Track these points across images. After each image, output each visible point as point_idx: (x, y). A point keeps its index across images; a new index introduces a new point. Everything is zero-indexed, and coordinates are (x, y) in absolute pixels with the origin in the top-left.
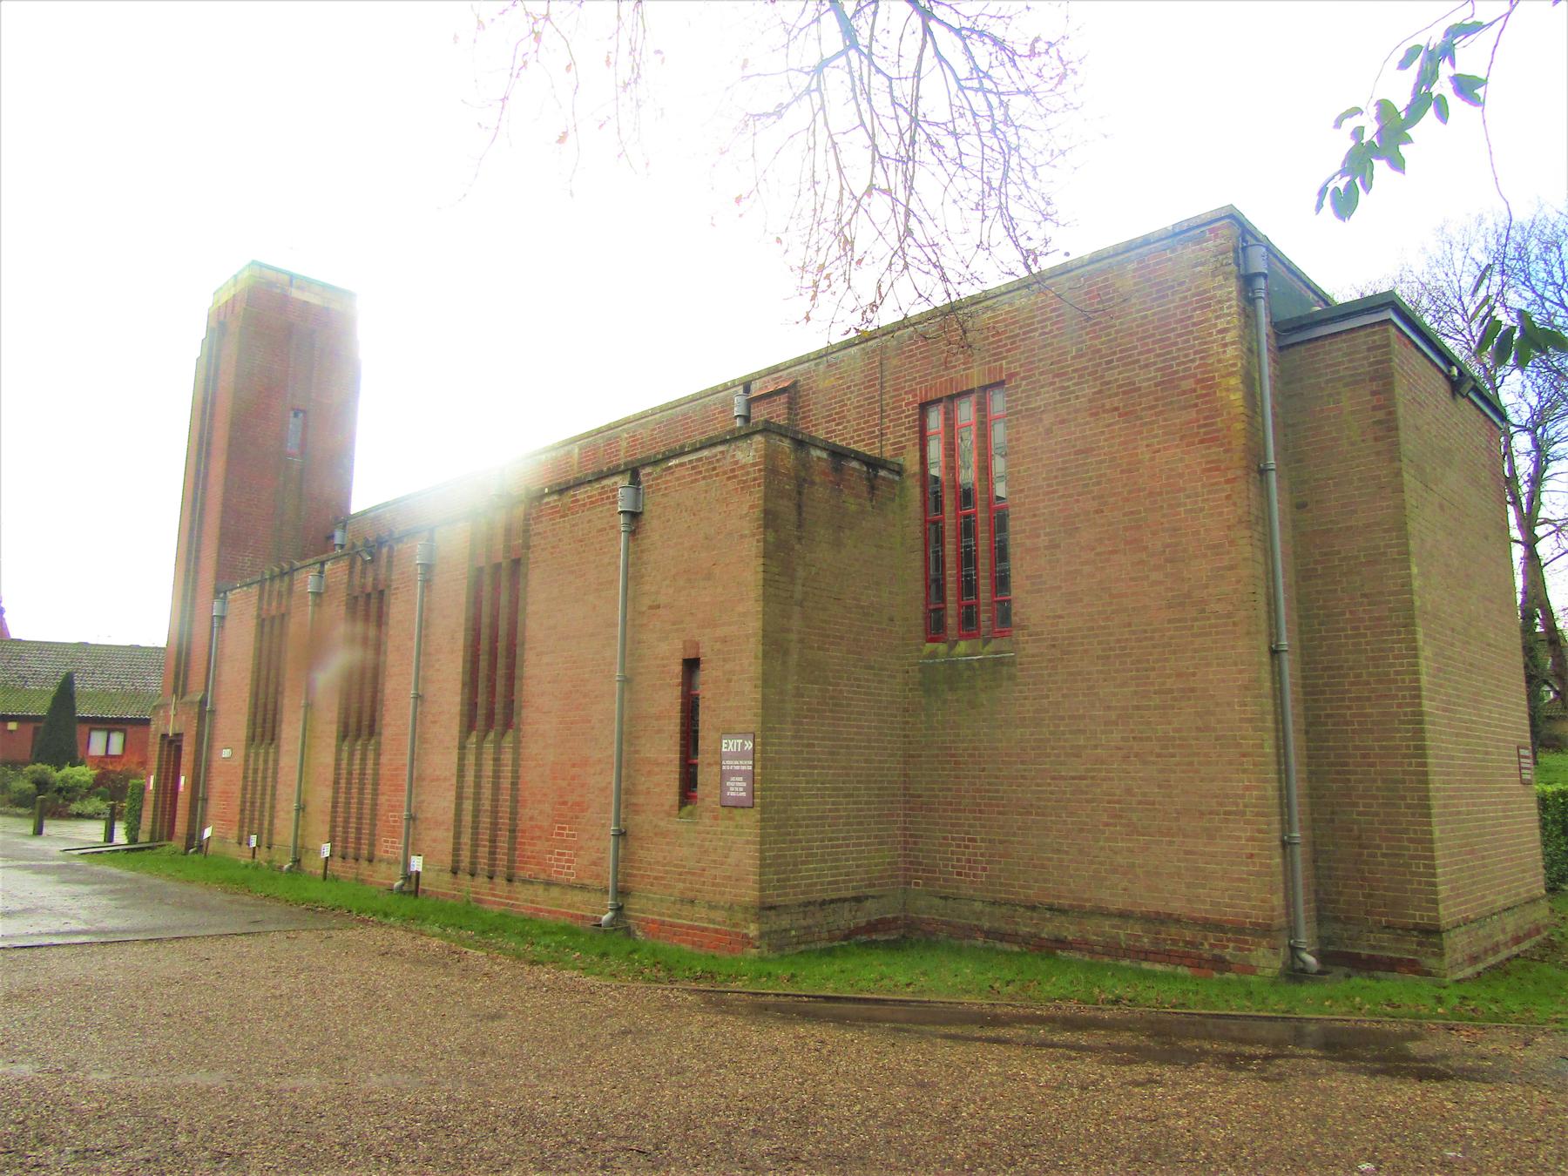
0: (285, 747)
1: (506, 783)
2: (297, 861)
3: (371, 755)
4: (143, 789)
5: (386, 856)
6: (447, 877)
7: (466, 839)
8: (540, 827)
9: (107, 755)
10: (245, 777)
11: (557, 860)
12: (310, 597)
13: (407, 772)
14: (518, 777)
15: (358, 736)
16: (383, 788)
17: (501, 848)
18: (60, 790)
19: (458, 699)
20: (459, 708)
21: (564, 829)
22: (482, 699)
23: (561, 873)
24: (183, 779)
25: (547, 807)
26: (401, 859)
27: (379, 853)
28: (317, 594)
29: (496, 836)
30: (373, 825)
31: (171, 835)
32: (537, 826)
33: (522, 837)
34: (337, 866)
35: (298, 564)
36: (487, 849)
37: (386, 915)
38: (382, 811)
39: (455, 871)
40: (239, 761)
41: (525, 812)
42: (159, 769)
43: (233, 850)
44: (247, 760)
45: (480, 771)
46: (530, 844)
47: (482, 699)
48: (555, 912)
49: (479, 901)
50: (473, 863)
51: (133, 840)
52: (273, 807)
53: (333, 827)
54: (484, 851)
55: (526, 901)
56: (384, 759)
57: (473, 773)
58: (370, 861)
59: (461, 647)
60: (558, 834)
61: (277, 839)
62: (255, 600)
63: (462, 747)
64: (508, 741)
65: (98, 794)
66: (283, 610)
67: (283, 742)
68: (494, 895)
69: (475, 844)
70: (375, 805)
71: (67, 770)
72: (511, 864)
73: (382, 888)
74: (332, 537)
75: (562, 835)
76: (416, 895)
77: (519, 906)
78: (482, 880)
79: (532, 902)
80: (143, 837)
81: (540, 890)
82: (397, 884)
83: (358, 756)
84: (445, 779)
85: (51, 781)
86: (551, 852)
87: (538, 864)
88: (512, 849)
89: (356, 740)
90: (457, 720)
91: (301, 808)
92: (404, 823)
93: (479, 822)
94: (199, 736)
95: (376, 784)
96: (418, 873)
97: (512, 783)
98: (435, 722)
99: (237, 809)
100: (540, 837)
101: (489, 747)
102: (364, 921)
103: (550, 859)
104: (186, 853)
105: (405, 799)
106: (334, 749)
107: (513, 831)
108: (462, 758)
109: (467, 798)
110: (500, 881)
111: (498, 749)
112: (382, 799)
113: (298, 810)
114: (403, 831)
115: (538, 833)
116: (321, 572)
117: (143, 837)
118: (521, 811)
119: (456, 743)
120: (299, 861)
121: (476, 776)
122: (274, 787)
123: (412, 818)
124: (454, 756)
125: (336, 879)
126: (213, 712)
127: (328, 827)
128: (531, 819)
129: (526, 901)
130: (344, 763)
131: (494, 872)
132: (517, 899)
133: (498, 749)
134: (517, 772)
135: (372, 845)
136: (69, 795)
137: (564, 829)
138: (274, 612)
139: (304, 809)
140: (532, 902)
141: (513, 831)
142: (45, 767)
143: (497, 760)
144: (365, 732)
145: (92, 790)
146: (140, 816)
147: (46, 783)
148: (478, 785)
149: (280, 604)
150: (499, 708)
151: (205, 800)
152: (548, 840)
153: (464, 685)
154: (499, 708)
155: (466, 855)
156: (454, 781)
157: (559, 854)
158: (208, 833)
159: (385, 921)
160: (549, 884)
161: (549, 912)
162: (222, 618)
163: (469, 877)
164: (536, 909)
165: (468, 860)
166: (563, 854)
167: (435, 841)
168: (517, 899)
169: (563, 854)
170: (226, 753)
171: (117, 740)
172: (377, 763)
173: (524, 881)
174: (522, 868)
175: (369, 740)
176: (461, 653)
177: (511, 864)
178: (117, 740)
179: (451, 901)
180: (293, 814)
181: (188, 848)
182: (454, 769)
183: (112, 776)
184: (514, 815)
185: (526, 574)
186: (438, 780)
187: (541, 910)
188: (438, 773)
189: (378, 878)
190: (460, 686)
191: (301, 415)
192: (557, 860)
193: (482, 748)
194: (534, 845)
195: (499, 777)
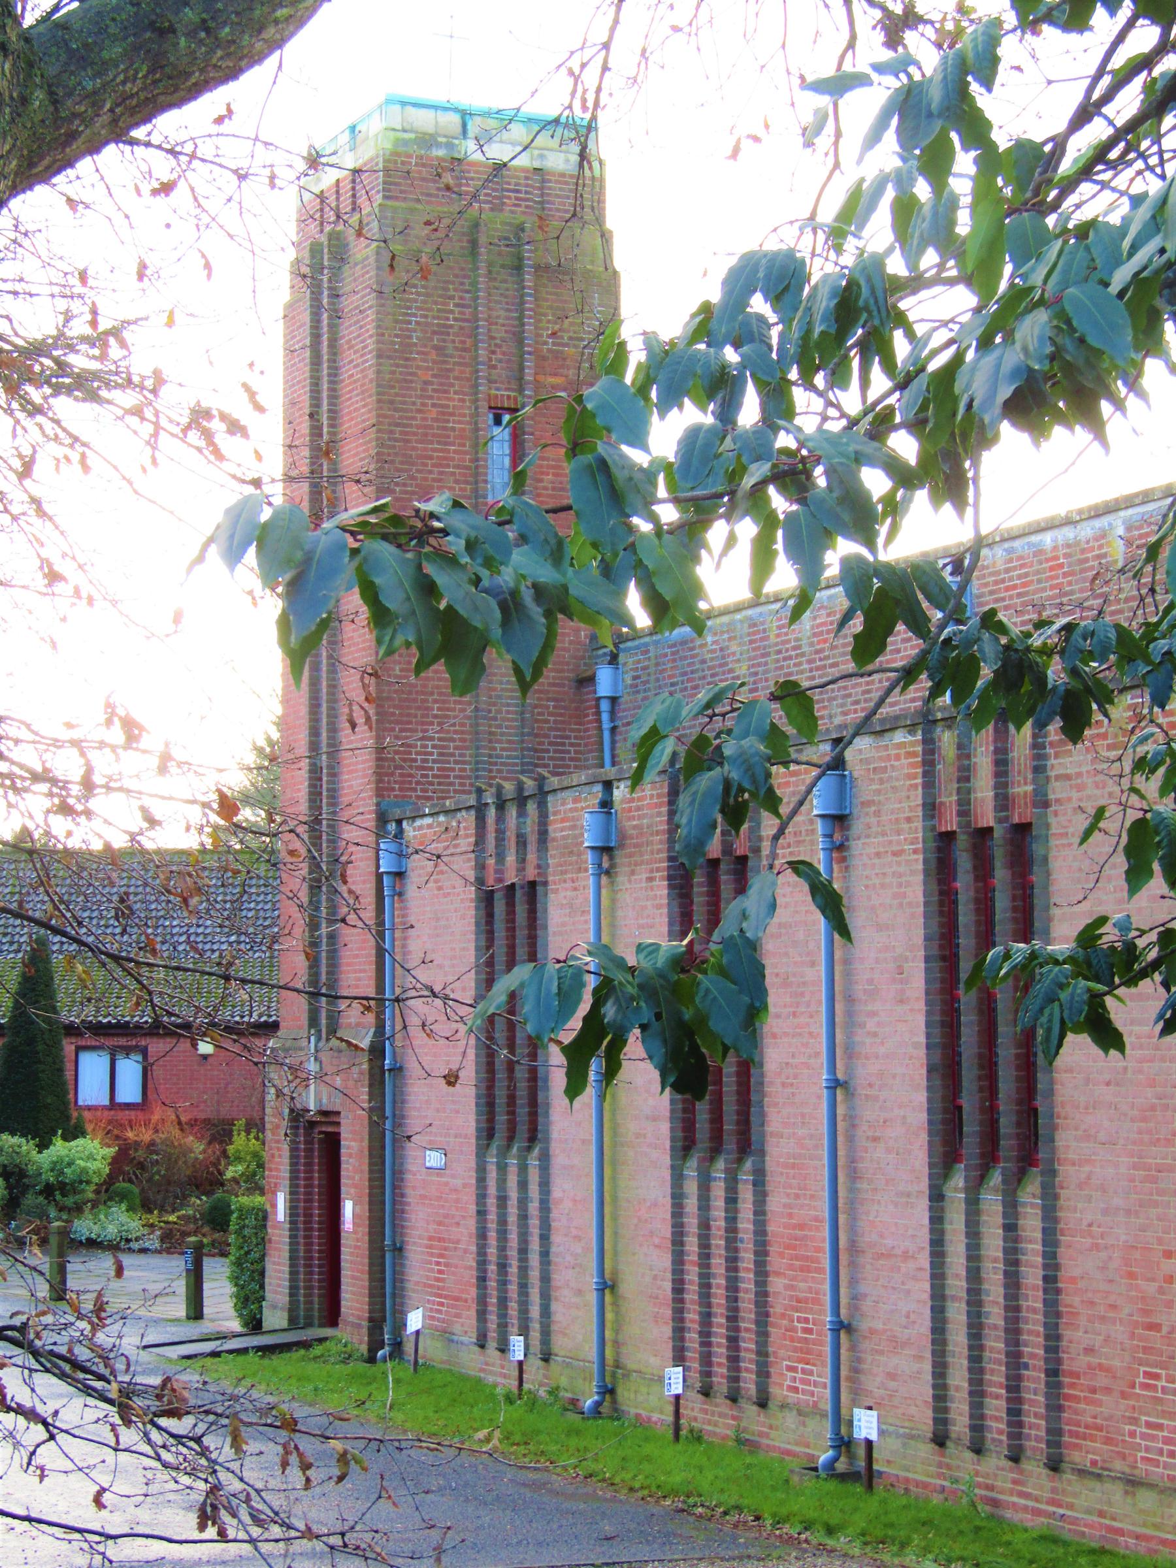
0: (559, 1159)
1: (1032, 1276)
2: (608, 1391)
3: (746, 1195)
4: (263, 1217)
5: (792, 1397)
6: (926, 1449)
7: (958, 1378)
8: (1106, 1369)
9: (114, 1105)
10: (481, 1213)
11: (1144, 1436)
12: (589, 856)
13: (826, 1233)
14: (1057, 1267)
15: (716, 1150)
16: (775, 1262)
17: (1033, 1403)
18: (48, 1191)
19: (921, 1097)
20: (924, 1116)
21: (1156, 1377)
22: (969, 1102)
23: (1156, 1463)
24: (348, 1209)
25: (1119, 1332)
26: (828, 1406)
27: (779, 1392)
28: (605, 850)
29: (1019, 1378)
30: (763, 1334)
31: (332, 1316)
32: (1101, 1367)
33: (1072, 1386)
34: (694, 1408)
35: (554, 782)
36: (1003, 1404)
37: (830, 1531)
38: (777, 1306)
39: (940, 1440)
40: (464, 1172)
41: (1075, 1338)
42: (294, 1178)
43: (471, 1360)
44: (481, 1180)
45: (978, 1246)
46: (1088, 1401)
47: (969, 1102)
48: (1147, 1538)
49: (995, 1503)
50: (978, 1428)
51: (254, 1325)
52: (546, 1279)
53: (679, 1331)
54: (996, 1407)
55: (1088, 1511)
56: (775, 1203)
57: (962, 1248)
58: (763, 1403)
59: (921, 993)
60: (1146, 1386)
61: (560, 1344)
62: (466, 842)
63: (937, 1197)
64: (1030, 1194)
65: (123, 1197)
66: (531, 873)
67: (555, 1148)
68: (1022, 1494)
69: (977, 1393)
70: (762, 1296)
71: (59, 1148)
72: (1055, 1435)
73: (794, 1464)
74: (591, 680)
75: (1154, 1388)
76: (870, 1487)
77: (1075, 1521)
78: (995, 1463)
79: (1101, 1514)
80: (275, 1318)
81: (1116, 1491)
82: (824, 1457)
83: (718, 1191)
84: (906, 1256)
85: (31, 1169)
86: (1134, 1421)
87: (1108, 1441)
88: (1055, 1407)
89: (712, 1159)
90: (924, 1137)
91: (607, 1286)
92: (828, 1338)
93: (981, 1348)
94: (377, 1112)
95: (762, 1251)
96: (869, 1443)
97: (1046, 1279)
98: (875, 1139)
99: (471, 1276)
100: (1108, 1390)
101: (992, 1203)
102: (790, 1540)
103: (1132, 1434)
104: (371, 1359)
105: (827, 1287)
106: (667, 1174)
107: (1053, 1372)
108: (937, 1219)
109: (954, 1298)
110: (1034, 1468)
111: (1011, 1207)
112: (777, 1284)
113: (601, 1290)
114: (828, 1349)
115: (1102, 1380)
116: (606, 804)
117: (275, 1318)
118: (1067, 1333)
119: (924, 1185)
120: (612, 1391)
121: (970, 1258)
122: (545, 1238)
123: (841, 1327)
124: (922, 1208)
125: (697, 1437)
126: (397, 1070)
127: (667, 1331)
128: (1089, 1350)
129: (1088, 1511)
130: (691, 1204)
131: (1020, 1448)
132: (1071, 1507)
133: (1011, 1207)
134: (1054, 1255)
135: (763, 1373)
136: (69, 1201)
137: (1156, 1377)
138: (511, 878)
139: (613, 1288)
140: (1101, 1514)
141: (1053, 1372)
142: (16, 1140)
143: (1011, 1228)
144: (730, 1143)
145: (108, 1191)
146: (262, 1273)
147: (22, 1174)
148: (974, 1275)
149: (522, 861)
150: (1007, 1124)
151: (399, 1250)
152: (1123, 1395)
153: (931, 1070)
154: (1007, 1124)
155: (521, 910)
156: (924, 1260)
157: (1149, 1425)
158: (415, 1320)
159: (830, 1542)
160: (1133, 1483)
161: (1138, 1537)
162: (400, 875)
163: (969, 1455)
164: (1110, 1529)
165: (966, 1420)
166: (1159, 1427)
167: (892, 1376)
168: (1071, 1507)
169: (1159, 1427)
170: (434, 1159)
171: (130, 1070)
172: (760, 1211)
173: (1082, 1473)
174: (1077, 1447)
175: (740, 1161)
176: (921, 1006)
177: (1055, 1435)
178: (130, 1070)
179: (936, 1499)
180: (592, 1298)
181: (375, 1345)
182: (924, 1236)
183: (140, 1154)
184: (1053, 1340)
185: (1045, 859)
186: (889, 1256)
187: (1120, 1532)
188: (889, 1242)
189: (779, 1439)
190: (924, 1071)
191: (506, 418)
192: (1144, 1436)
193: (976, 1201)
194: (1099, 1403)
195: (1017, 1263)
